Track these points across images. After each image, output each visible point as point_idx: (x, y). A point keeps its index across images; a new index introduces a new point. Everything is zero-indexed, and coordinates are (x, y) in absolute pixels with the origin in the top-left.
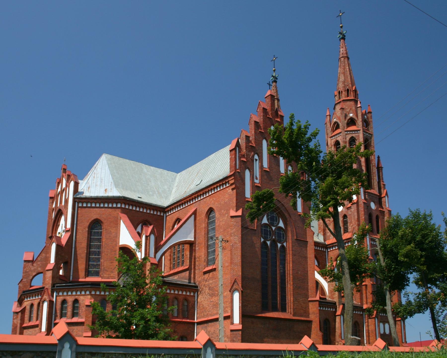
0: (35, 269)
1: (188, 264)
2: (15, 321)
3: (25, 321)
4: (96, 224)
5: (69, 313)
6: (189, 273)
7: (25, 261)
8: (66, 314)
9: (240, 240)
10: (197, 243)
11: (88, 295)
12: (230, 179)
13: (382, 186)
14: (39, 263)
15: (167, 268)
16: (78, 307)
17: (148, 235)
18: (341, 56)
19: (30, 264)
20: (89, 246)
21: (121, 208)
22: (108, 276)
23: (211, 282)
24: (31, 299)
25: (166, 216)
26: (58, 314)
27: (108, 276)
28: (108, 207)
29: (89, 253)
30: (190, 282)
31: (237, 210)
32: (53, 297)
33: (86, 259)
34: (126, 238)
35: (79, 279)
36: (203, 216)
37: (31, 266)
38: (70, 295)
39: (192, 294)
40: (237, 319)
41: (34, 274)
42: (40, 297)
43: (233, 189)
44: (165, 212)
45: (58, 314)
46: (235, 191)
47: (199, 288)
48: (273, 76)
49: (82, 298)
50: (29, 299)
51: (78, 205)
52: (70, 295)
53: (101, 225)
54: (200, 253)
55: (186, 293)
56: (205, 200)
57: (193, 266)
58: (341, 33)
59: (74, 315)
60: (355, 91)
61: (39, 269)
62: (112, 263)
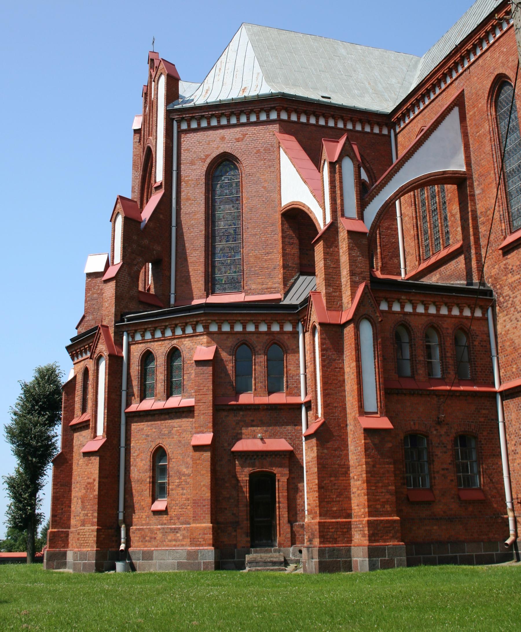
1: (460, 237)
5: (160, 387)
6: (465, 259)
7: (89, 275)
8: (153, 387)
10: (475, 176)
15: (412, 260)
17: (336, 159)
21: (279, 121)
22: (260, 287)
25: (396, 135)
26: (136, 390)
27: (260, 287)
30: (470, 283)
34: (296, 186)
35: (192, 299)
36: (483, 102)
39: (478, 314)
44: (392, 126)
45: (136, 390)
49: (187, 342)
51: (179, 127)
52: (159, 340)
53: (236, 168)
55: (461, 311)
56: (480, 61)
57: (472, 238)
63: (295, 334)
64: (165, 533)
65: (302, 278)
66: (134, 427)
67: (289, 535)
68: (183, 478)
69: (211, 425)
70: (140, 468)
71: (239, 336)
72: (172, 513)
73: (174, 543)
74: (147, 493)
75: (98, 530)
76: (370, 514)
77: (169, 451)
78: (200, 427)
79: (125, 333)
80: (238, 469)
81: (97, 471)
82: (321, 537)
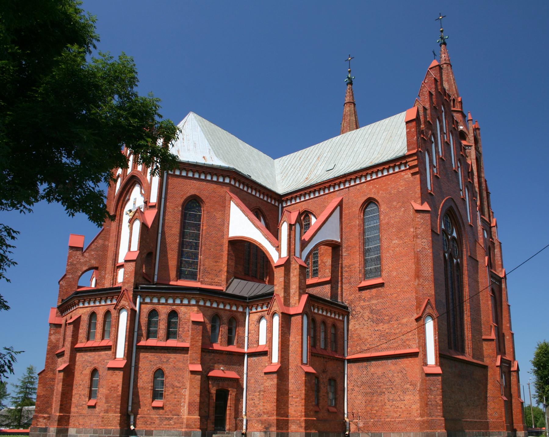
0: (86, 261)
2: (53, 337)
3: (79, 340)
4: (193, 204)
7: (71, 248)
9: (430, 245)
10: (344, 245)
11: (194, 305)
12: (411, 159)
13: (491, 213)
14: (93, 253)
16: (175, 323)
18: (444, 62)
19: (79, 253)
20: (182, 234)
21: (229, 184)
23: (374, 302)
24: (92, 304)
25: (283, 207)
26: (144, 332)
27: (210, 280)
28: (211, 181)
29: (182, 244)
31: (422, 203)
32: (135, 304)
33: (179, 252)
35: (170, 281)
36: (356, 209)
37: (80, 257)
38: (163, 304)
40: (431, 359)
41: (85, 268)
42: (114, 302)
43: (413, 174)
46: (418, 176)
47: (350, 310)
48: (348, 77)
50: (86, 305)
53: (200, 206)
54: (352, 260)
56: (358, 187)
58: (442, 38)
59: (170, 335)
60: (461, 102)
61: (93, 262)
62: (216, 262)
63: (244, 314)
64: (161, 420)
65: (235, 280)
66: (142, 355)
67: (234, 425)
68: (175, 389)
69: (199, 359)
70: (145, 380)
71: (214, 310)
72: (166, 409)
73: (168, 426)
74: (149, 395)
75: (121, 416)
76: (306, 416)
77: (166, 372)
78: (193, 359)
79: (139, 296)
80: (211, 386)
81: (121, 380)
82: (277, 426)
